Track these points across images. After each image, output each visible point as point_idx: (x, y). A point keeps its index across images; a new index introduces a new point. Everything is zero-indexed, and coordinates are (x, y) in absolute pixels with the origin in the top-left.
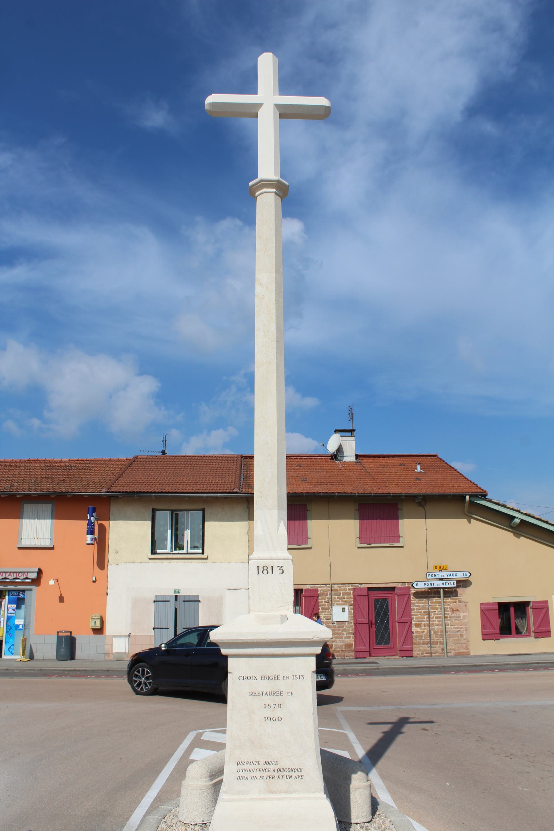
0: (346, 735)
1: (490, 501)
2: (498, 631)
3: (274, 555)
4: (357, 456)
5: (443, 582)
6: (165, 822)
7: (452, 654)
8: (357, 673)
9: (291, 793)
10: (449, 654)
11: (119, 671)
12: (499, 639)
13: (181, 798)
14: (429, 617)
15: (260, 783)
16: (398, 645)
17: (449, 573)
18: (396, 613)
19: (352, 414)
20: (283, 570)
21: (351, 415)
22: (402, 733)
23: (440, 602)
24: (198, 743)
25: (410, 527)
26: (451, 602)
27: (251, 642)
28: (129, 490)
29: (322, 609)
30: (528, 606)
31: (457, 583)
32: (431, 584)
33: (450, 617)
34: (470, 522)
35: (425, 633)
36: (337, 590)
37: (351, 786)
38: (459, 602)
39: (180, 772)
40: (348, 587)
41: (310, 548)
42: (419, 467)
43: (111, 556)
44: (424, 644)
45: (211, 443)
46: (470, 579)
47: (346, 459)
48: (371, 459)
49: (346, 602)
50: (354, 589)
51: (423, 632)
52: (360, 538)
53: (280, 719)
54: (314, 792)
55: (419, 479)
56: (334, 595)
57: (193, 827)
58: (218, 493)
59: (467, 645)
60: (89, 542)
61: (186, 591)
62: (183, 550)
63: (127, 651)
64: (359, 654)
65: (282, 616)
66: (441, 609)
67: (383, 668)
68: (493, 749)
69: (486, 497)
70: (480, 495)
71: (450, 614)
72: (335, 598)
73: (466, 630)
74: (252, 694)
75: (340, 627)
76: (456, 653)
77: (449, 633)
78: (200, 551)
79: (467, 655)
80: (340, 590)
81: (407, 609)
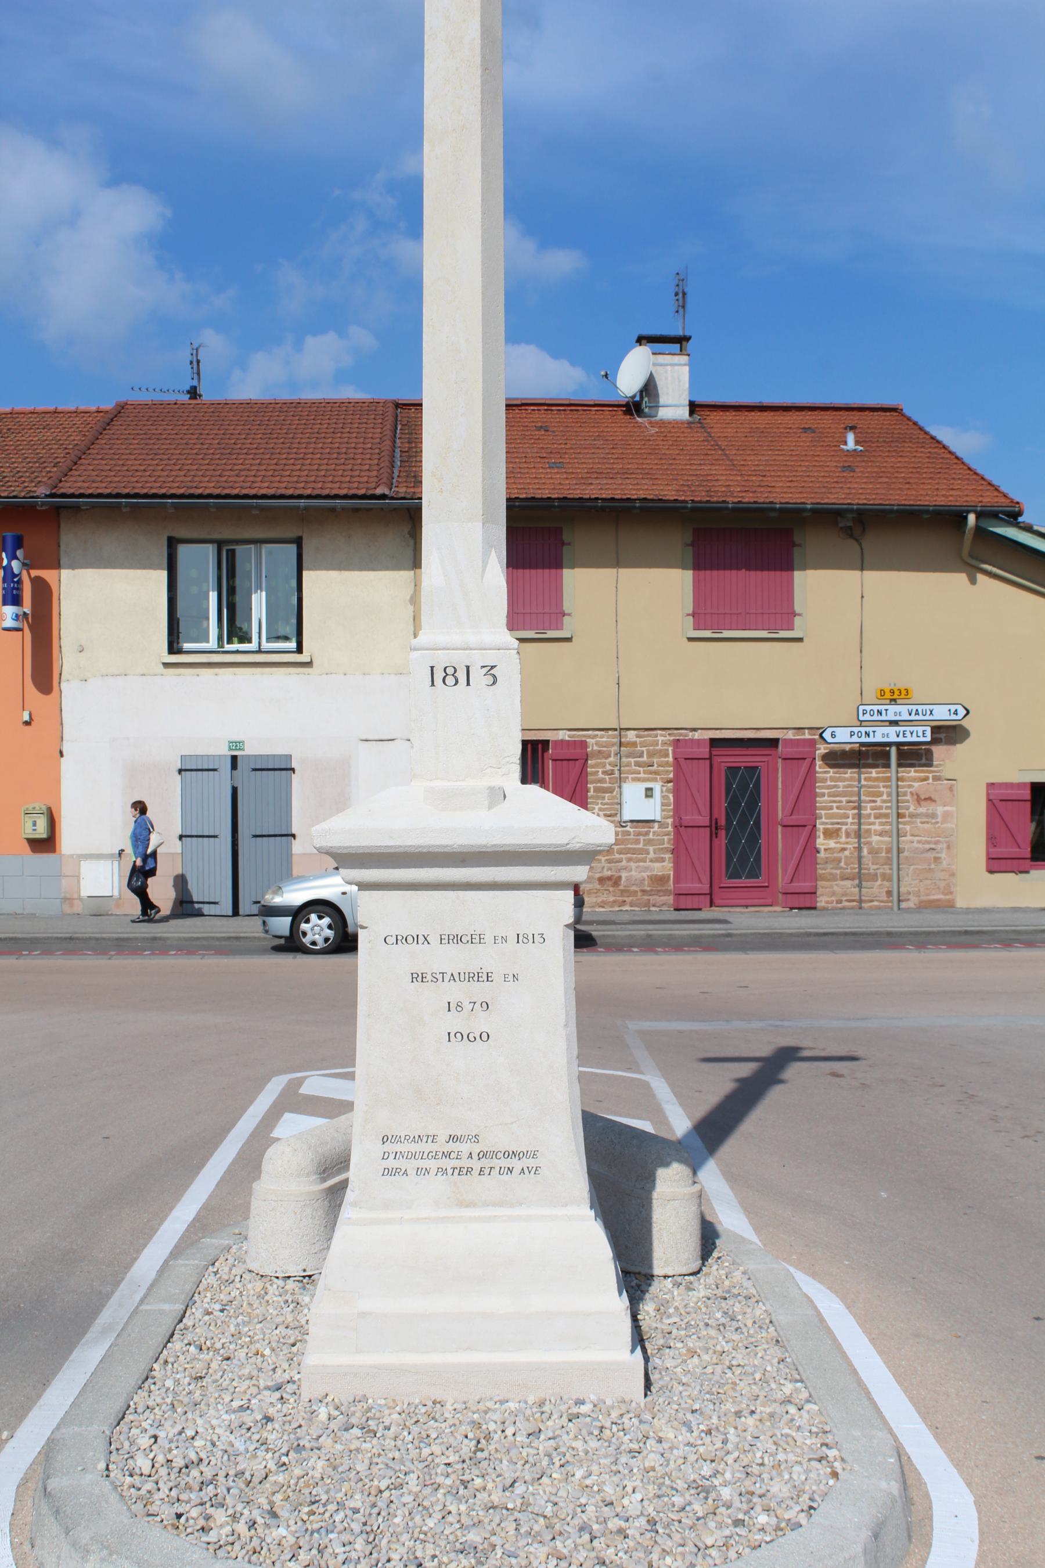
0: (646, 1085)
1: (1029, 529)
2: (1027, 852)
3: (471, 639)
4: (693, 407)
5: (898, 729)
6: (216, 1273)
7: (911, 904)
8: (677, 946)
9: (511, 1206)
10: (903, 905)
11: (97, 939)
12: (1027, 872)
13: (252, 1220)
14: (859, 816)
15: (438, 1185)
17: (914, 708)
18: (778, 802)
19: (684, 294)
20: (494, 676)
21: (681, 296)
22: (781, 1081)
23: (888, 779)
24: (293, 1101)
25: (825, 592)
26: (915, 780)
28: (108, 491)
29: (596, 790)
31: (932, 733)
32: (867, 734)
33: (912, 816)
34: (973, 581)
35: (847, 853)
37: (655, 1195)
38: (936, 778)
39: (249, 1164)
40: (661, 738)
41: (569, 640)
42: (851, 438)
43: (68, 659)
44: (843, 878)
45: (313, 369)
46: (964, 723)
47: (665, 414)
48: (729, 415)
49: (656, 773)
50: (677, 743)
51: (843, 849)
52: (694, 615)
54: (565, 1205)
55: (850, 468)
56: (627, 757)
57: (280, 1282)
58: (336, 497)
59: (948, 885)
60: (9, 623)
61: (259, 744)
62: (250, 641)
63: (116, 893)
64: (684, 900)
65: (491, 789)
66: (889, 794)
67: (741, 935)
68: (995, 1119)
69: (1020, 519)
70: (1004, 513)
71: (911, 810)
72: (629, 765)
73: (948, 847)
74: (418, 977)
75: (639, 834)
76: (921, 902)
77: (906, 854)
78: (292, 645)
79: (948, 906)
80: (643, 745)
81: (805, 794)
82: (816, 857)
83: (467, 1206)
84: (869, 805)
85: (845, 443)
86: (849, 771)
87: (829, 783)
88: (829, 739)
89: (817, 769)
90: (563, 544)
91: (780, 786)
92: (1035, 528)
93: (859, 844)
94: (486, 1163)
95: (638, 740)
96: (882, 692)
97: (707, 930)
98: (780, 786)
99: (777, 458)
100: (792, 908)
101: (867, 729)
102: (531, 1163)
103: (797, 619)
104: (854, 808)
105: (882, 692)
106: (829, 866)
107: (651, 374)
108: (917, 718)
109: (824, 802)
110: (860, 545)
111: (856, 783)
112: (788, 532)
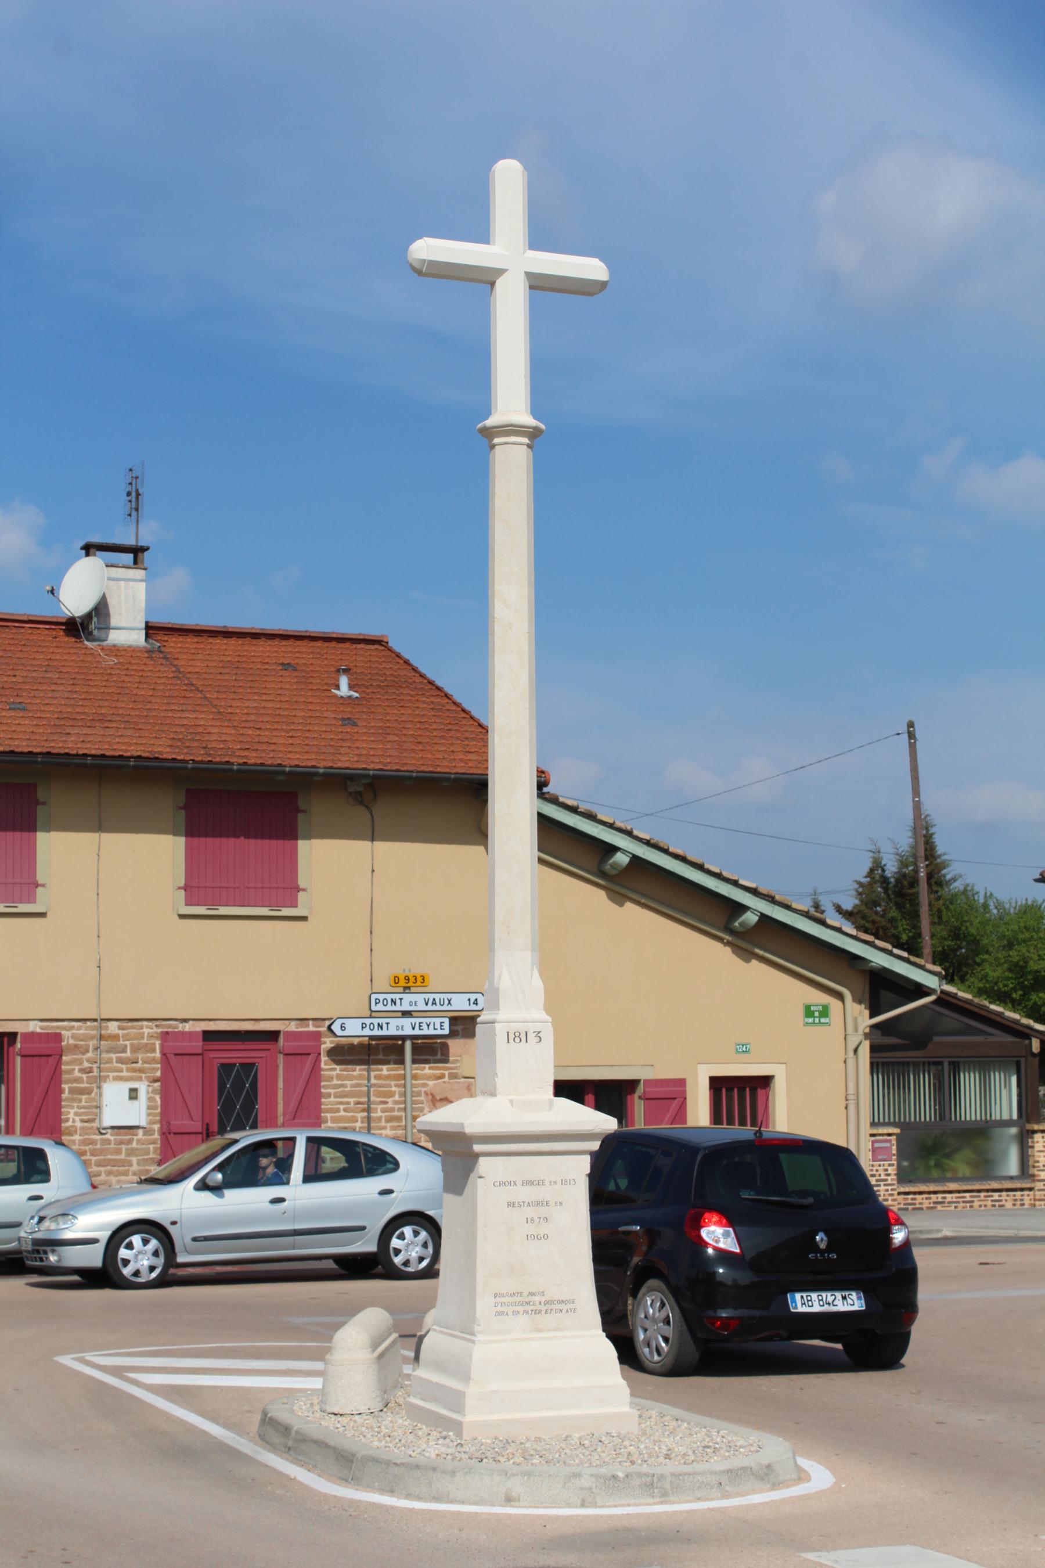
4: (151, 630)
5: (413, 1020)
14: (369, 1119)
17: (431, 996)
19: (138, 494)
21: (135, 498)
25: (329, 863)
29: (72, 1091)
32: (380, 1026)
36: (116, 1037)
38: (453, 1076)
41: (43, 915)
42: (344, 681)
47: (115, 637)
48: (190, 641)
49: (141, 1071)
50: (165, 1036)
52: (186, 888)
53: (546, 1237)
55: (350, 722)
56: (108, 1051)
72: (110, 1061)
74: (511, 1205)
75: (121, 1142)
80: (126, 1038)
85: (338, 687)
86: (358, 1067)
87: (335, 1082)
88: (338, 1032)
89: (323, 1066)
90: (37, 803)
91: (281, 1084)
92: (561, 799)
94: (548, 1307)
95: (121, 1032)
96: (396, 980)
98: (281, 1084)
99: (266, 704)
101: (380, 1021)
102: (572, 1306)
103: (301, 894)
104: (363, 1110)
105: (396, 980)
107: (104, 596)
108: (434, 1008)
111: (366, 1082)
112: (293, 797)
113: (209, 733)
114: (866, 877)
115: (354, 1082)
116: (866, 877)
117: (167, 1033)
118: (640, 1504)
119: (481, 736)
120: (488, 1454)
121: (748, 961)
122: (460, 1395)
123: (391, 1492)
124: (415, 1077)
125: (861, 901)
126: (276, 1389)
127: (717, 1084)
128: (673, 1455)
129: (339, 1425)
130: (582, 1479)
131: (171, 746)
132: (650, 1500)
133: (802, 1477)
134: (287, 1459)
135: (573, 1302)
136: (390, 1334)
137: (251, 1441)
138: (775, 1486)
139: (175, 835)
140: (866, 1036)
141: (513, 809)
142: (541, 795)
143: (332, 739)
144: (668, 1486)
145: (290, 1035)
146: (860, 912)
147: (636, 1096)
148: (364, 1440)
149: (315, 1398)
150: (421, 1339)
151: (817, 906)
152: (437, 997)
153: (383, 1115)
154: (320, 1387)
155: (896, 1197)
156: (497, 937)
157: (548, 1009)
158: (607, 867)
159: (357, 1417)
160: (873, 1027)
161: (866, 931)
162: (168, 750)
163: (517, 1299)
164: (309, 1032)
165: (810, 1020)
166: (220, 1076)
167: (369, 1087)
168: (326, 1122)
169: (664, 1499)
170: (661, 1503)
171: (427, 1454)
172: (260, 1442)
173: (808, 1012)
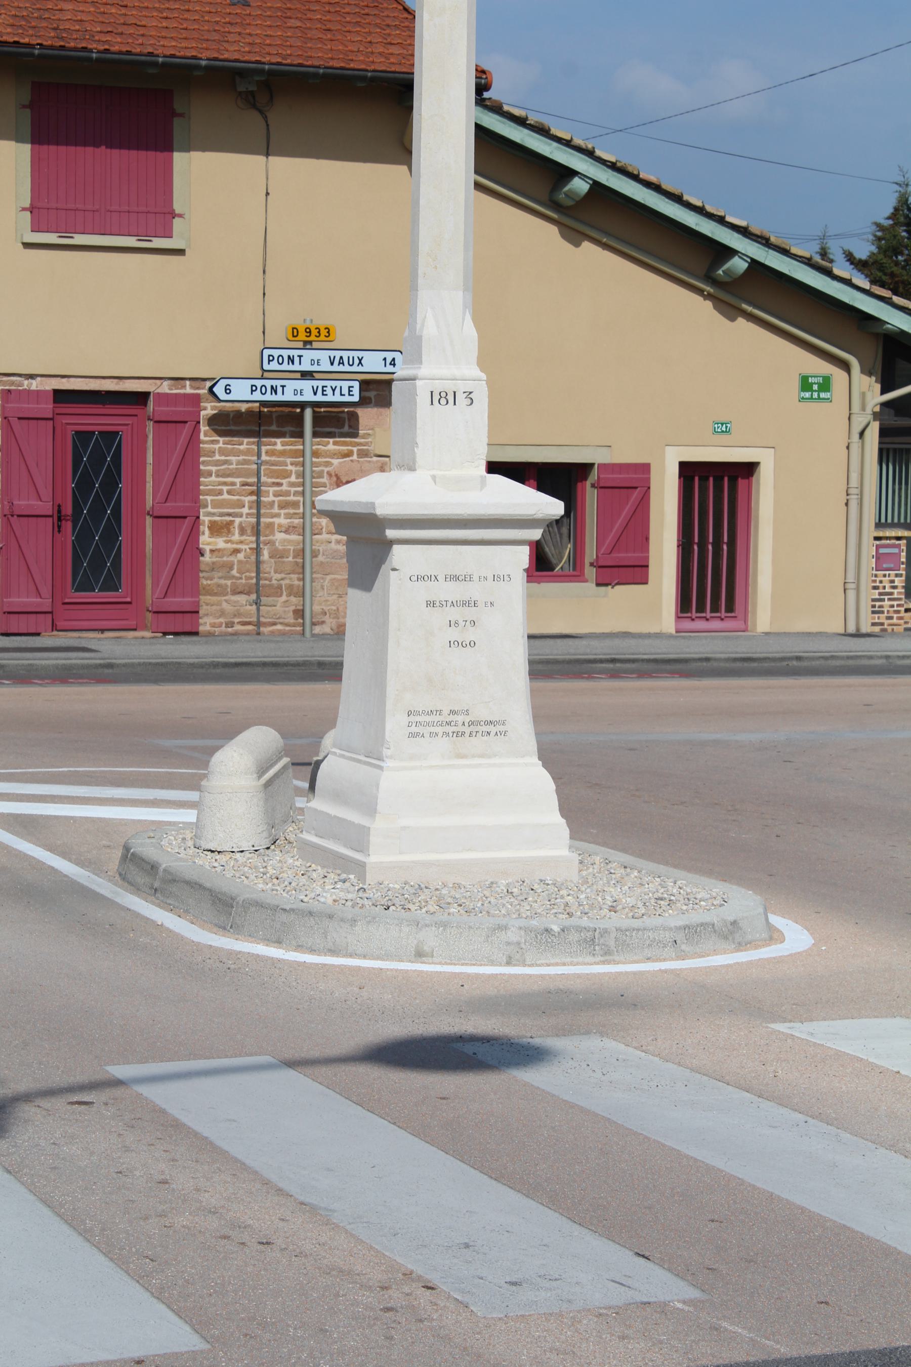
5: (315, 383)
9: (490, 757)
14: (258, 504)
15: (443, 744)
16: (150, 594)
17: (338, 354)
25: (211, 180)
26: (334, 455)
27: (413, 520)
30: (585, 478)
32: (274, 390)
35: (241, 556)
38: (363, 454)
44: (236, 592)
51: (236, 551)
52: (32, 209)
67: (125, 665)
74: (431, 604)
77: (321, 558)
82: (198, 561)
83: (462, 758)
84: (272, 490)
86: (246, 440)
87: (217, 457)
88: (222, 395)
89: (202, 437)
91: (150, 459)
93: (258, 545)
94: (473, 728)
97: (75, 659)
98: (150, 459)
100: (165, 634)
101: (274, 383)
103: (176, 222)
104: (252, 493)
105: (295, 332)
106: (216, 574)
108: (341, 368)
109: (210, 484)
110: (266, 118)
111: (256, 458)
113: (61, 10)
114: (888, 218)
115: (241, 458)
116: (888, 218)
117: (9, 391)
118: (577, 964)
119: (407, 24)
120: (397, 901)
121: (732, 319)
122: (364, 831)
123: (279, 942)
124: (315, 454)
125: (879, 247)
126: (139, 821)
127: (688, 470)
128: (619, 907)
129: (216, 864)
130: (509, 933)
131: (12, 25)
132: (590, 959)
133: (774, 936)
134: (153, 903)
135: (504, 724)
136: (280, 758)
137: (110, 881)
138: (741, 946)
139: (17, 141)
140: (876, 416)
141: (444, 119)
142: (481, 101)
143: (217, 22)
144: (612, 943)
145: (160, 396)
146: (875, 262)
147: (588, 483)
148: (246, 881)
149: (188, 832)
150: (318, 764)
151: (824, 254)
152: (345, 355)
153: (276, 499)
154: (193, 819)
155: (902, 614)
156: (420, 272)
157: (482, 363)
158: (561, 197)
159: (238, 855)
160: (884, 405)
161: (883, 285)
162: (9, 30)
163: (436, 718)
164: (185, 395)
165: (807, 395)
166: (75, 446)
167: (259, 465)
168: (206, 506)
169: (607, 958)
170: (603, 962)
171: (322, 900)
172: (120, 882)
173: (805, 384)
